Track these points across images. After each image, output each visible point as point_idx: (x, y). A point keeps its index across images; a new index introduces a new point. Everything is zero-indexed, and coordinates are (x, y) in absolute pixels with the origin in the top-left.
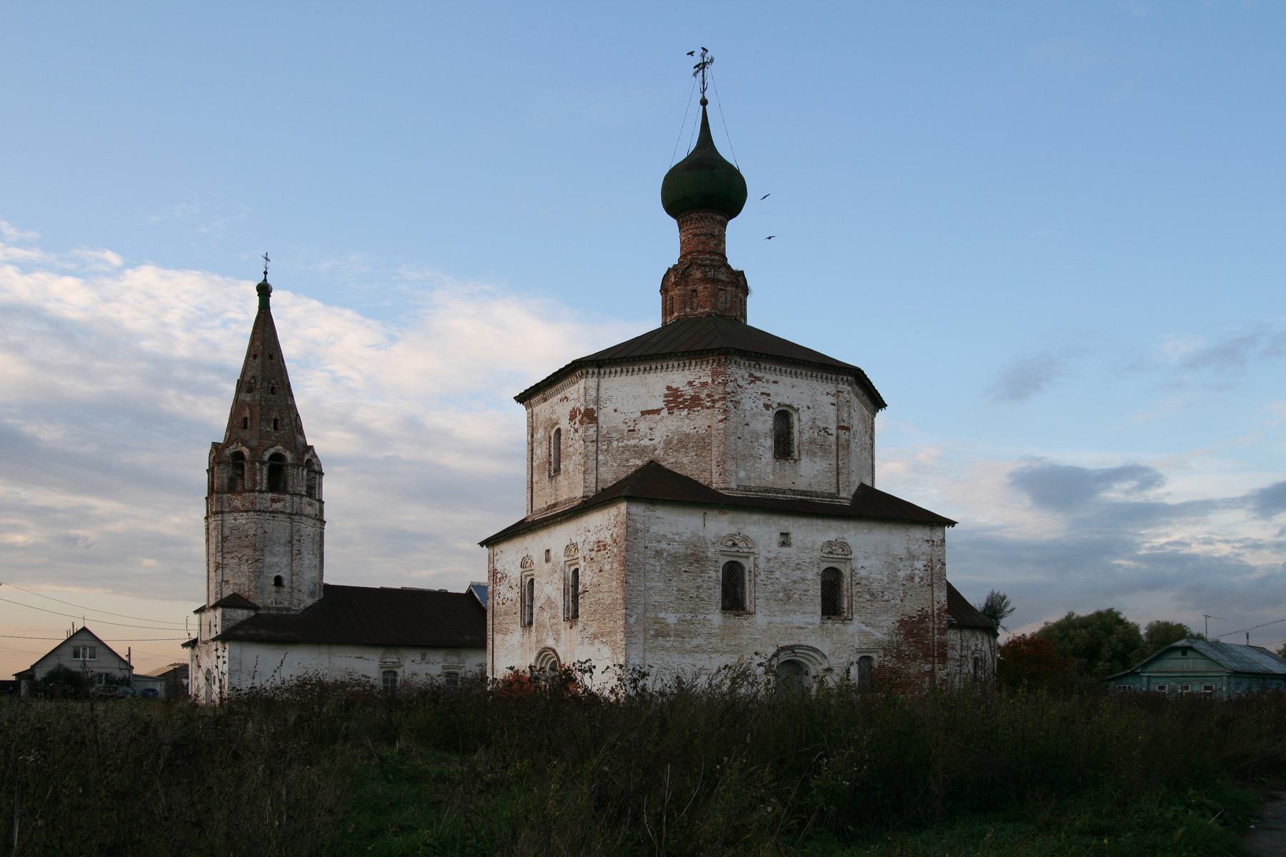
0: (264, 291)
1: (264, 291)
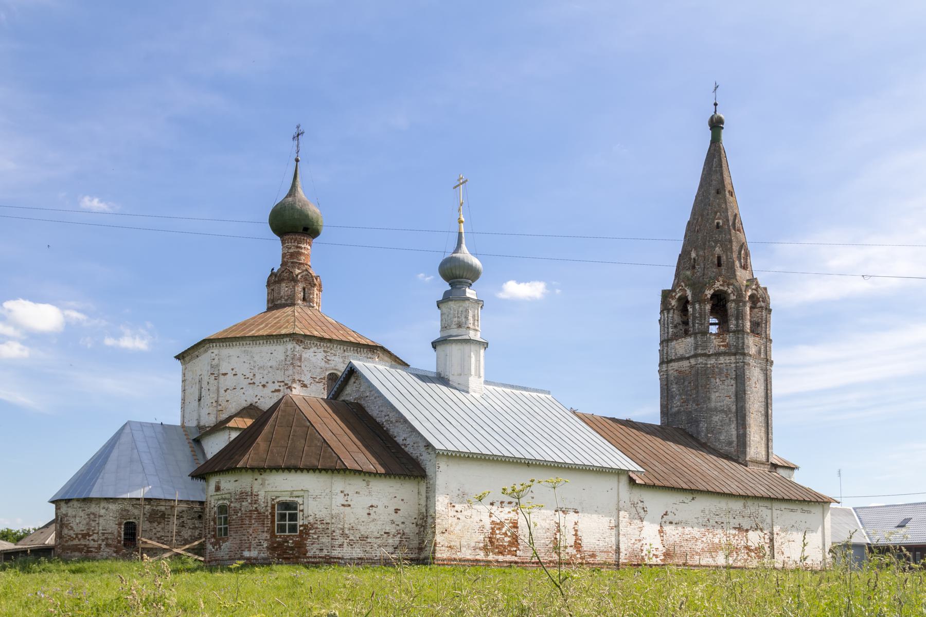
0: (716, 125)
1: (716, 125)
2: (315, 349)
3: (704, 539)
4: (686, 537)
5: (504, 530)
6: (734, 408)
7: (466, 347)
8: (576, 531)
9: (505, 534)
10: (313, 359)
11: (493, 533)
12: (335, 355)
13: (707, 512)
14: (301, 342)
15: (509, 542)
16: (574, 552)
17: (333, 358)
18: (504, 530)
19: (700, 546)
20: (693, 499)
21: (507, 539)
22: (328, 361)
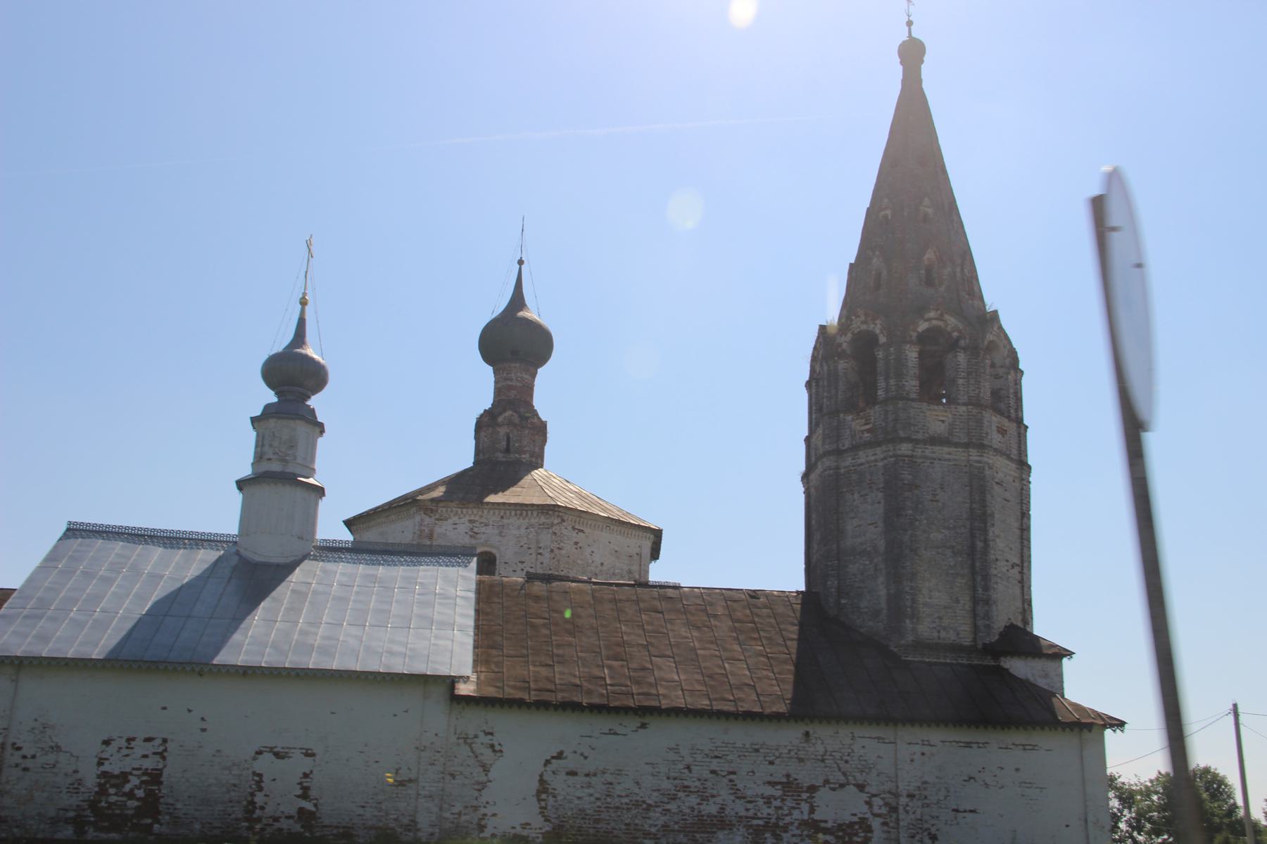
0: (912, 54)
1: (912, 54)
2: (456, 519)
3: (673, 807)
5: (127, 788)
6: (882, 545)
9: (131, 795)
11: (102, 791)
12: (486, 525)
14: (432, 511)
15: (137, 808)
17: (483, 530)
18: (127, 788)
19: (657, 818)
20: (643, 726)
21: (132, 804)
22: (474, 535)
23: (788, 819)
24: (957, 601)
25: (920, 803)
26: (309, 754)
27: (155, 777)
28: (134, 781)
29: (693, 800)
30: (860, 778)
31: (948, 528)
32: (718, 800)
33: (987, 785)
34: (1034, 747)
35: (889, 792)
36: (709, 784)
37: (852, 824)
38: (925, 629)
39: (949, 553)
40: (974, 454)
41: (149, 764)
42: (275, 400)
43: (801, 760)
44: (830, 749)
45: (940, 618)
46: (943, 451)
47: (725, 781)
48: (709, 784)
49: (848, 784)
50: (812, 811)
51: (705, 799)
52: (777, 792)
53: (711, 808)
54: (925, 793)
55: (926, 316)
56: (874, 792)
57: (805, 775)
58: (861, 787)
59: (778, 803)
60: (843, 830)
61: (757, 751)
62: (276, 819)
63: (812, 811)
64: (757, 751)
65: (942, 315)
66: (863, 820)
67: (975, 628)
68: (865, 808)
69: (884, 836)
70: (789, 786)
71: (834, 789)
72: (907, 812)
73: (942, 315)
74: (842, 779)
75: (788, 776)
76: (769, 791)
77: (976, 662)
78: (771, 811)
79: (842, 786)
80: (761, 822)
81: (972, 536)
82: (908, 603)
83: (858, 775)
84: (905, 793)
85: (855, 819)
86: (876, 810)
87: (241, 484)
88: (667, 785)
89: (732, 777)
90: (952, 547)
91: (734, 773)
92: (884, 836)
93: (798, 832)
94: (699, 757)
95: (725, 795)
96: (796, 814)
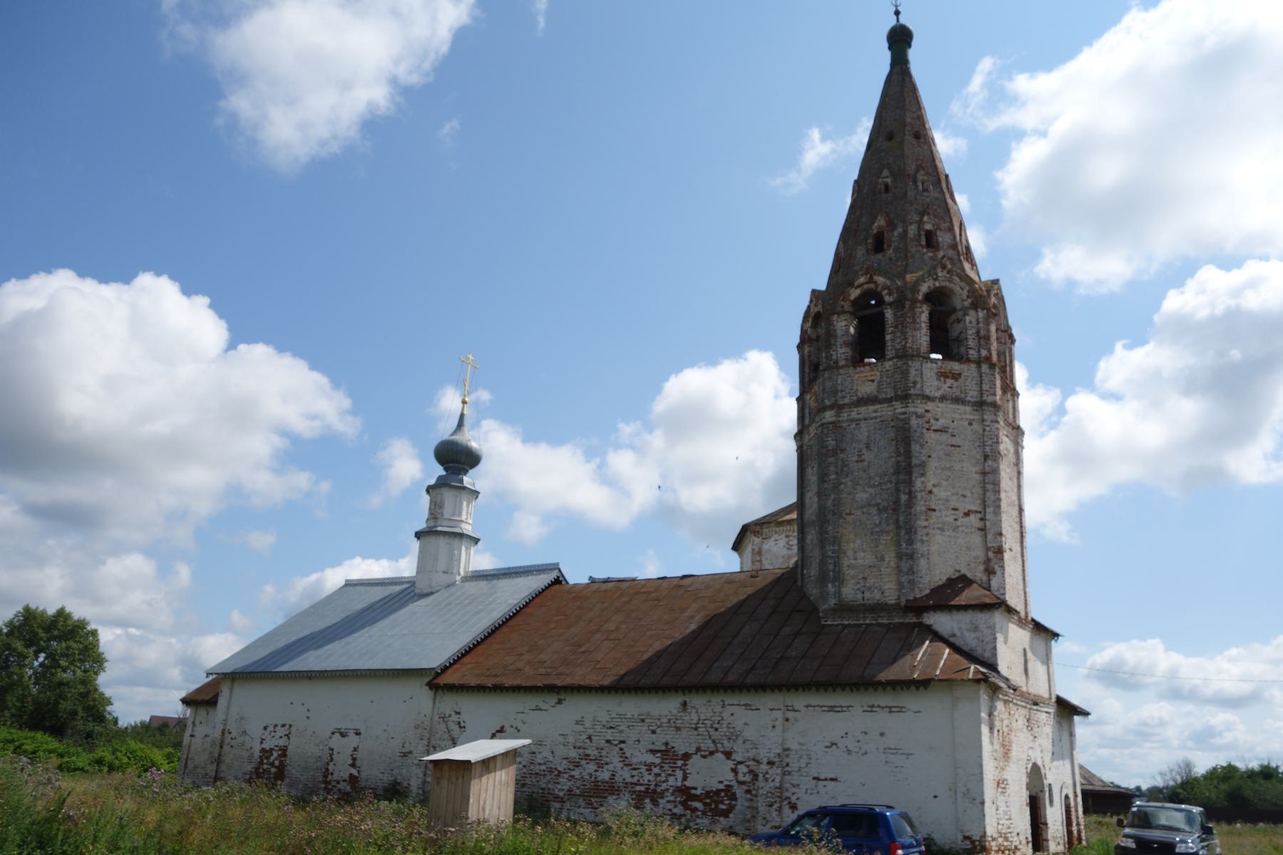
0: (900, 39)
1: (900, 39)
2: (776, 536)
3: (576, 773)
4: (537, 769)
7: (456, 541)
8: (354, 759)
10: (774, 549)
11: (261, 763)
13: (588, 724)
16: (348, 789)
19: (565, 784)
20: (560, 702)
21: (273, 770)
23: (664, 786)
24: (882, 559)
25: (779, 771)
26: (358, 734)
27: (284, 751)
28: (275, 754)
29: (592, 767)
30: (728, 745)
31: (874, 486)
32: (611, 767)
33: (849, 752)
34: (901, 710)
35: (754, 760)
36: (604, 753)
37: (718, 792)
38: (850, 592)
39: (874, 511)
40: (899, 407)
41: (281, 743)
42: (444, 473)
43: (678, 729)
44: (703, 717)
45: (864, 578)
46: (865, 411)
47: (617, 749)
48: (604, 753)
49: (717, 751)
50: (685, 778)
51: (600, 766)
52: (656, 760)
53: (605, 775)
54: (787, 760)
55: (856, 284)
56: (739, 759)
57: (681, 743)
58: (728, 755)
59: (656, 770)
60: (710, 797)
61: (643, 721)
62: (338, 782)
63: (685, 778)
64: (643, 721)
65: (871, 277)
66: (729, 787)
67: (900, 586)
68: (731, 776)
69: (747, 804)
70: (667, 753)
71: (704, 757)
72: (766, 780)
73: (871, 277)
74: (712, 747)
75: (667, 744)
76: (650, 758)
77: (897, 620)
78: (651, 778)
79: (712, 753)
80: (642, 788)
81: (898, 490)
82: (831, 567)
83: (725, 742)
84: (765, 761)
85: (721, 787)
86: (741, 778)
87: (418, 535)
88: (573, 754)
89: (622, 746)
90: (878, 505)
91: (623, 742)
92: (747, 804)
93: (672, 798)
94: (598, 728)
95: (616, 762)
96: (671, 781)
